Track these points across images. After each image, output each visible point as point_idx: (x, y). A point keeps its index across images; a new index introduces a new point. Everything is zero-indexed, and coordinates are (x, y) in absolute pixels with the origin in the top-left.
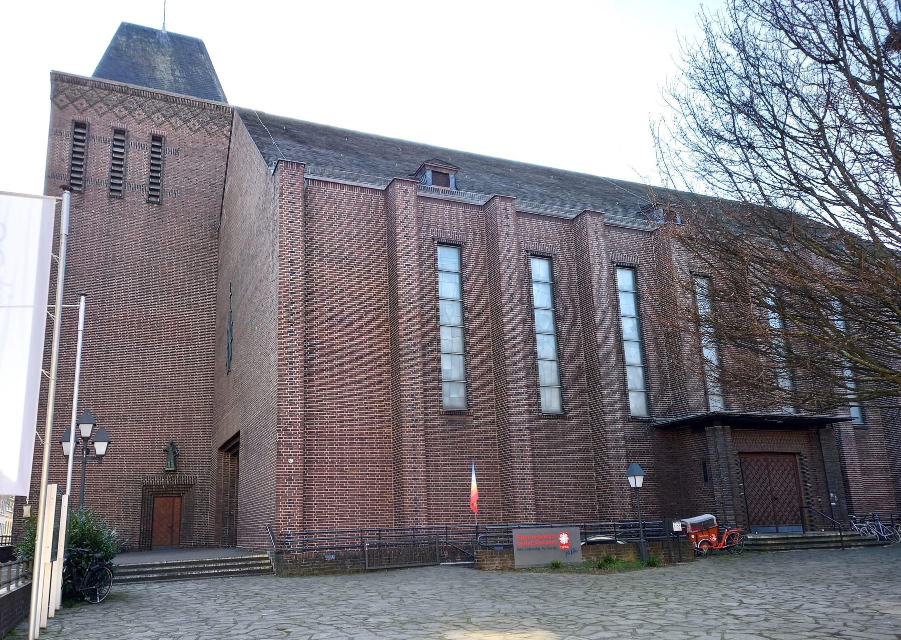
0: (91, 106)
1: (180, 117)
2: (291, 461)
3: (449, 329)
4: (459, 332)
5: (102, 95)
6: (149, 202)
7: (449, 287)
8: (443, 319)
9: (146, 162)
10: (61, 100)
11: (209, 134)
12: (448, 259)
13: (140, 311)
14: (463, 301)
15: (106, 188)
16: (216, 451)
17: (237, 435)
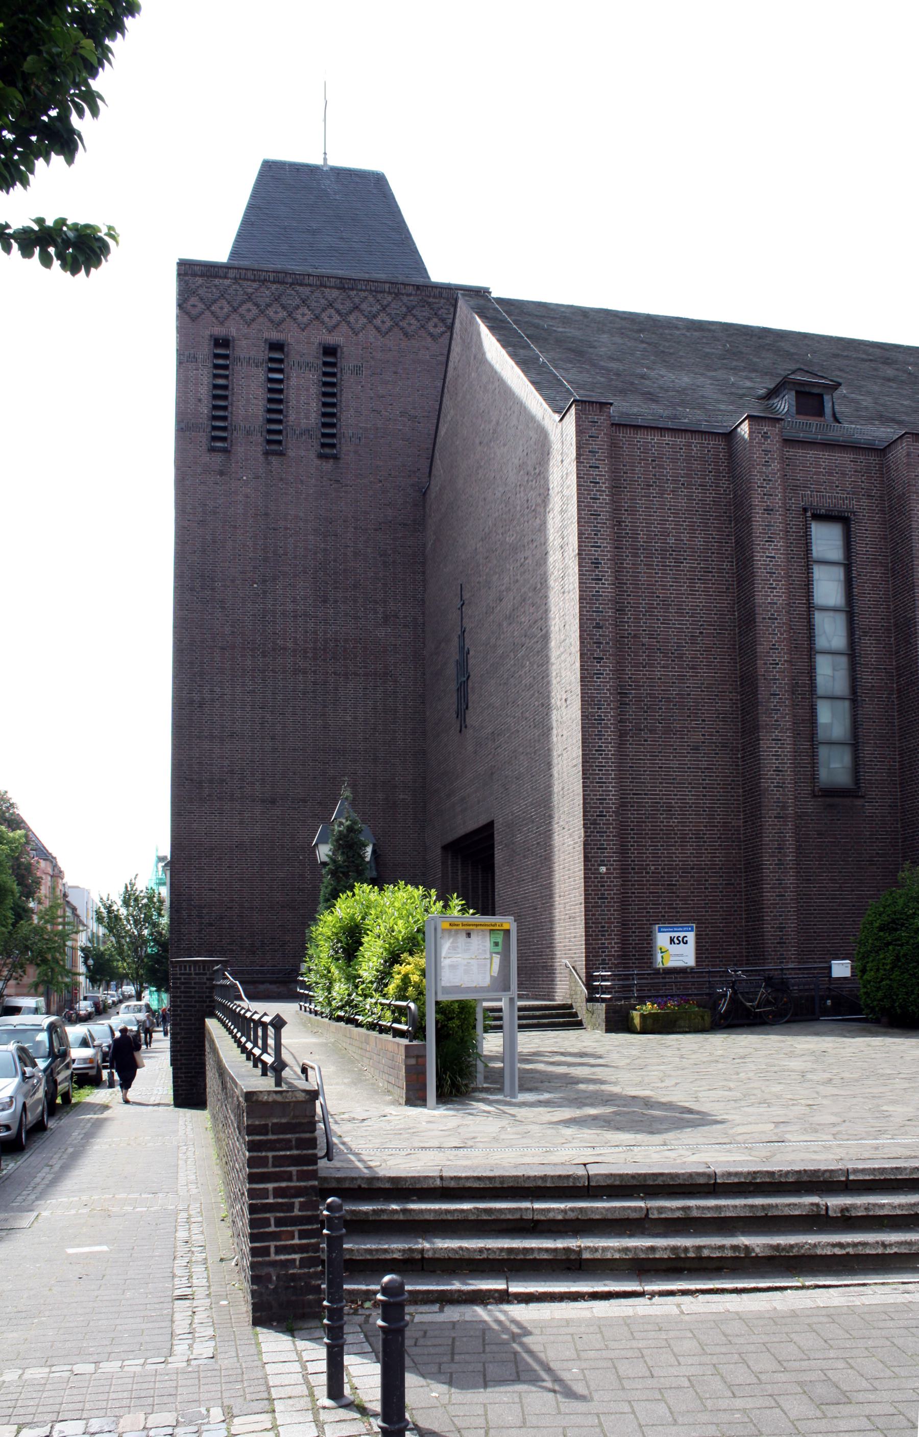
0: (235, 310)
1: (361, 311)
2: (603, 869)
3: (829, 657)
4: (843, 661)
5: (250, 290)
6: (321, 456)
7: (828, 588)
8: (821, 642)
9: (314, 390)
10: (194, 306)
11: (406, 334)
12: (826, 541)
13: (315, 633)
14: (850, 610)
15: (260, 440)
16: (439, 851)
17: (490, 825)
